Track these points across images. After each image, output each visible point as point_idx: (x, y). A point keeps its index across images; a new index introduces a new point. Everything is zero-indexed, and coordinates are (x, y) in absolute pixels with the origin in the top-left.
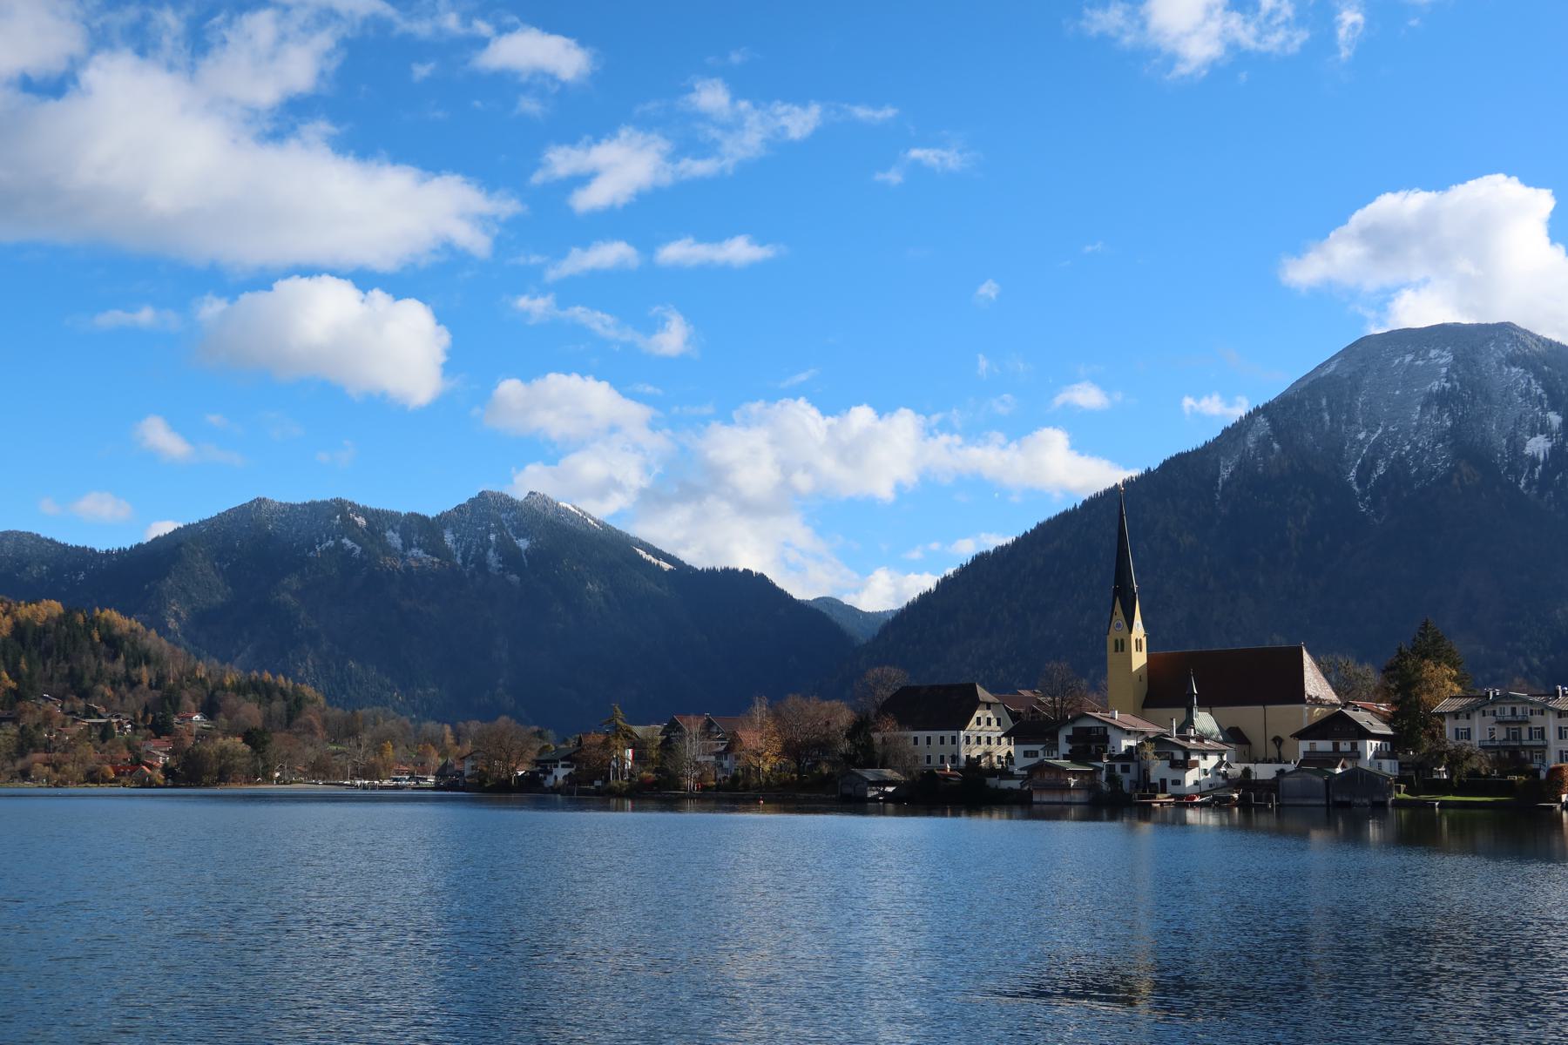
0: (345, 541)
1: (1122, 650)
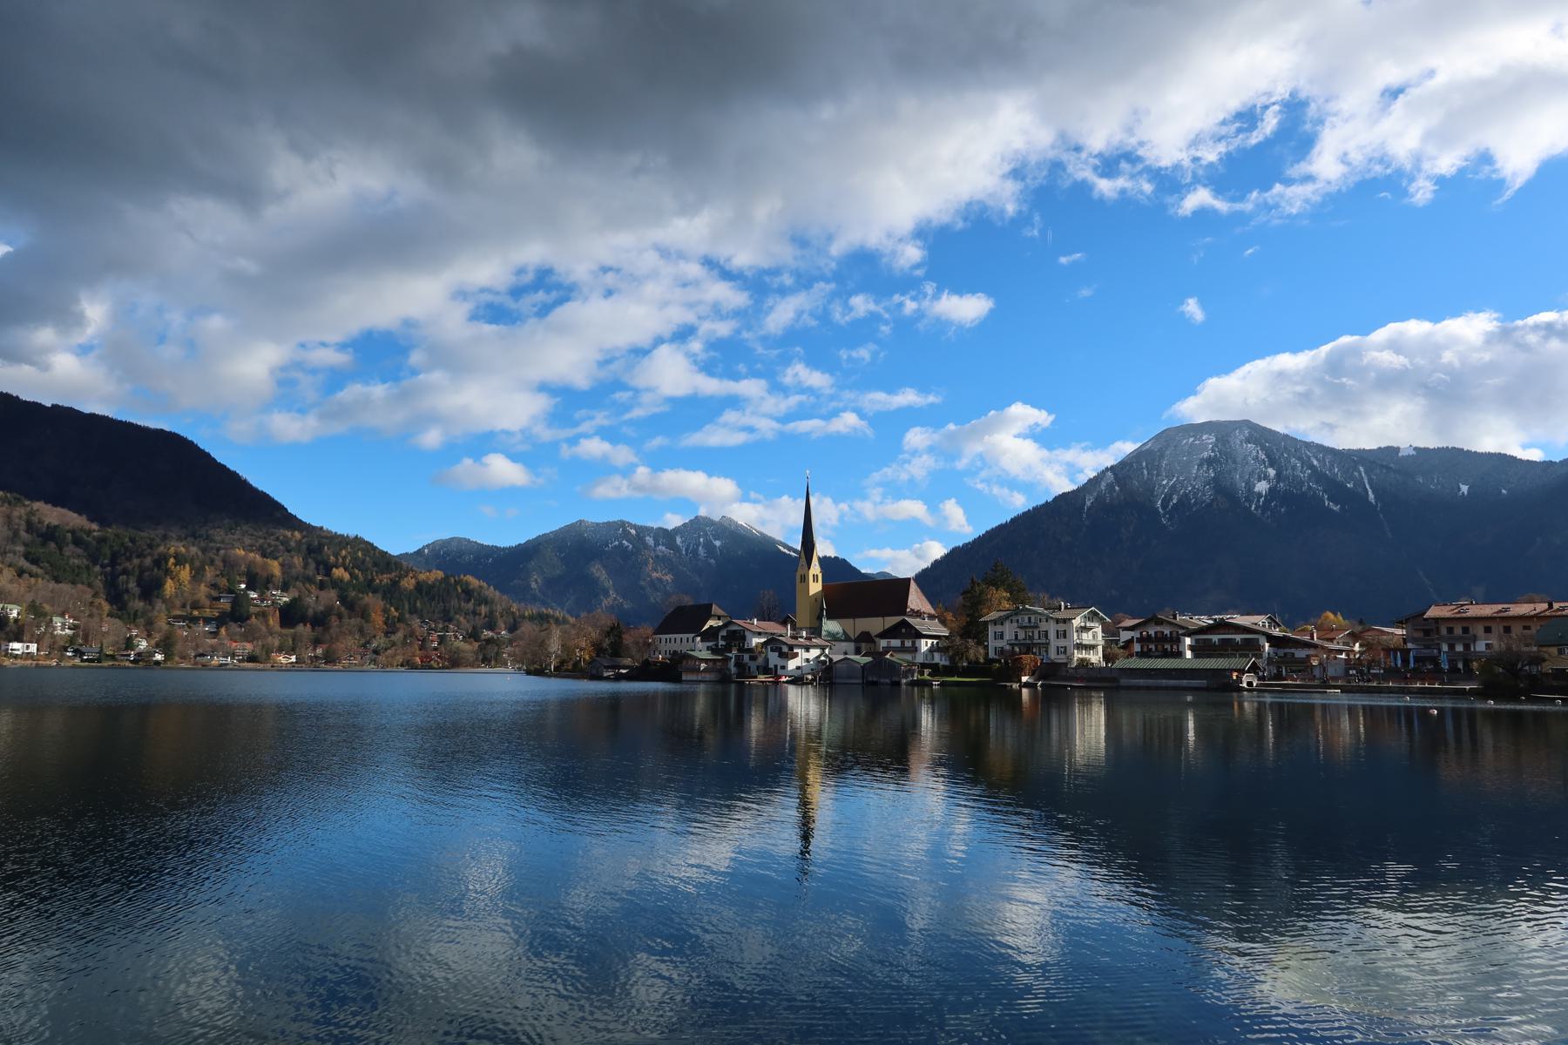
0: (624, 542)
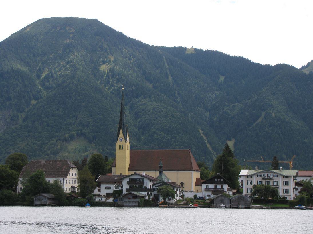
1: (122, 149)
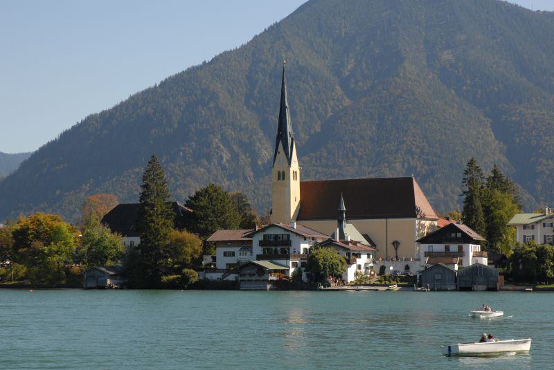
1: (283, 179)
